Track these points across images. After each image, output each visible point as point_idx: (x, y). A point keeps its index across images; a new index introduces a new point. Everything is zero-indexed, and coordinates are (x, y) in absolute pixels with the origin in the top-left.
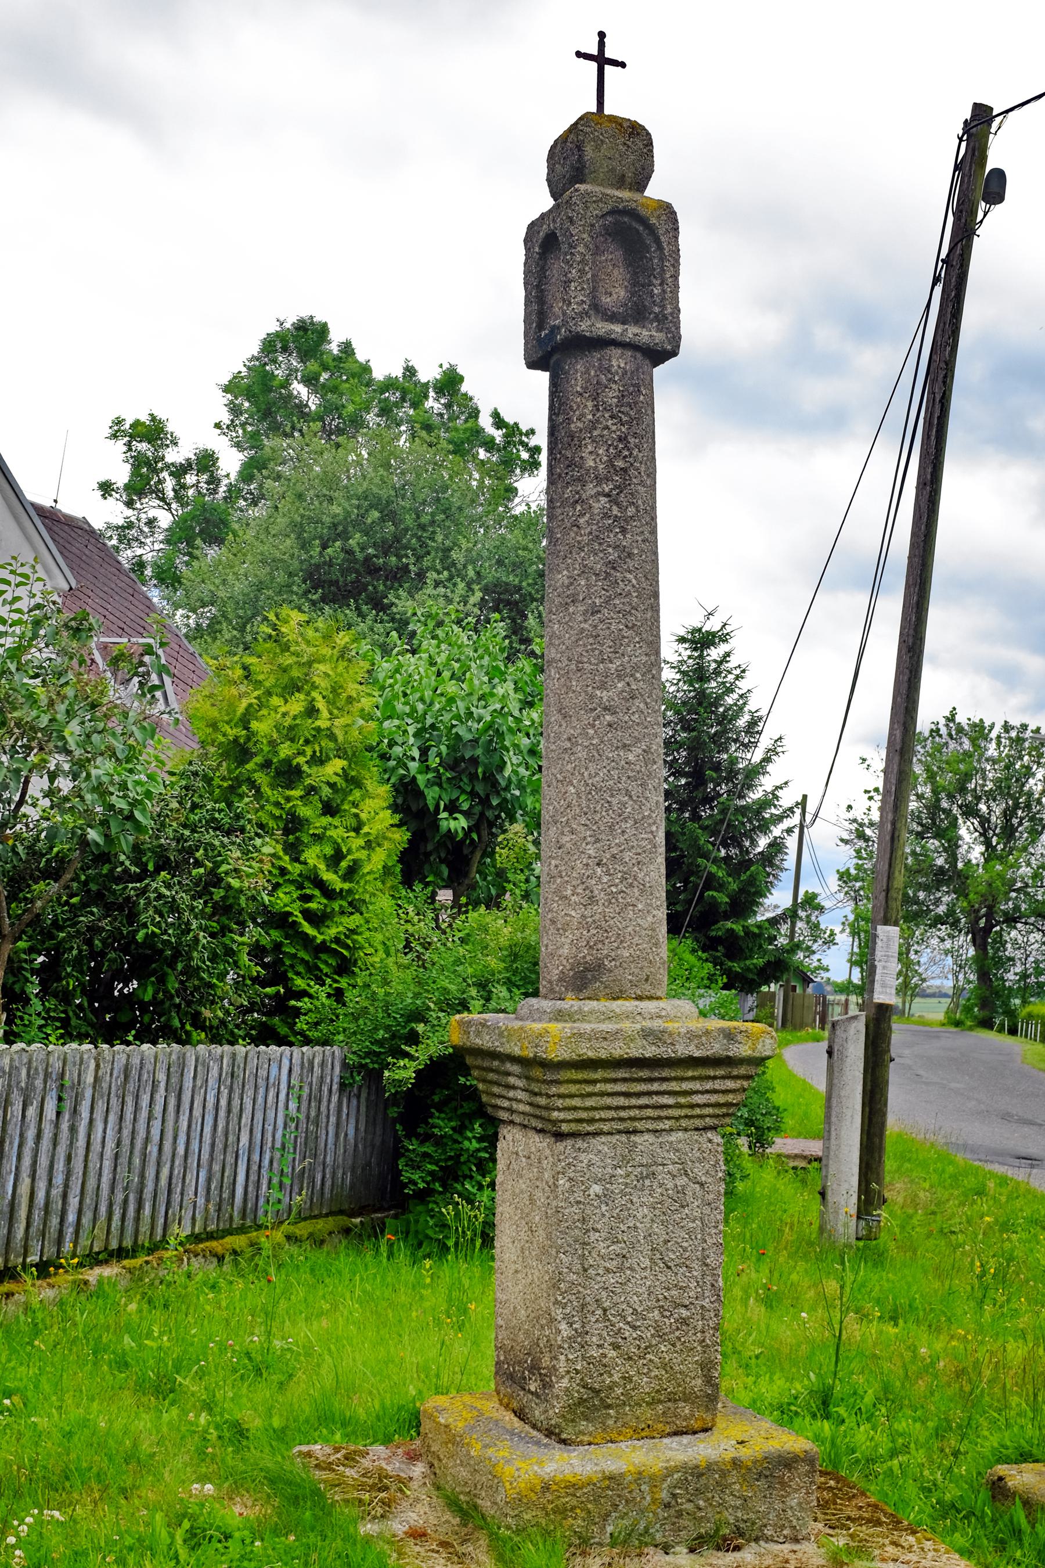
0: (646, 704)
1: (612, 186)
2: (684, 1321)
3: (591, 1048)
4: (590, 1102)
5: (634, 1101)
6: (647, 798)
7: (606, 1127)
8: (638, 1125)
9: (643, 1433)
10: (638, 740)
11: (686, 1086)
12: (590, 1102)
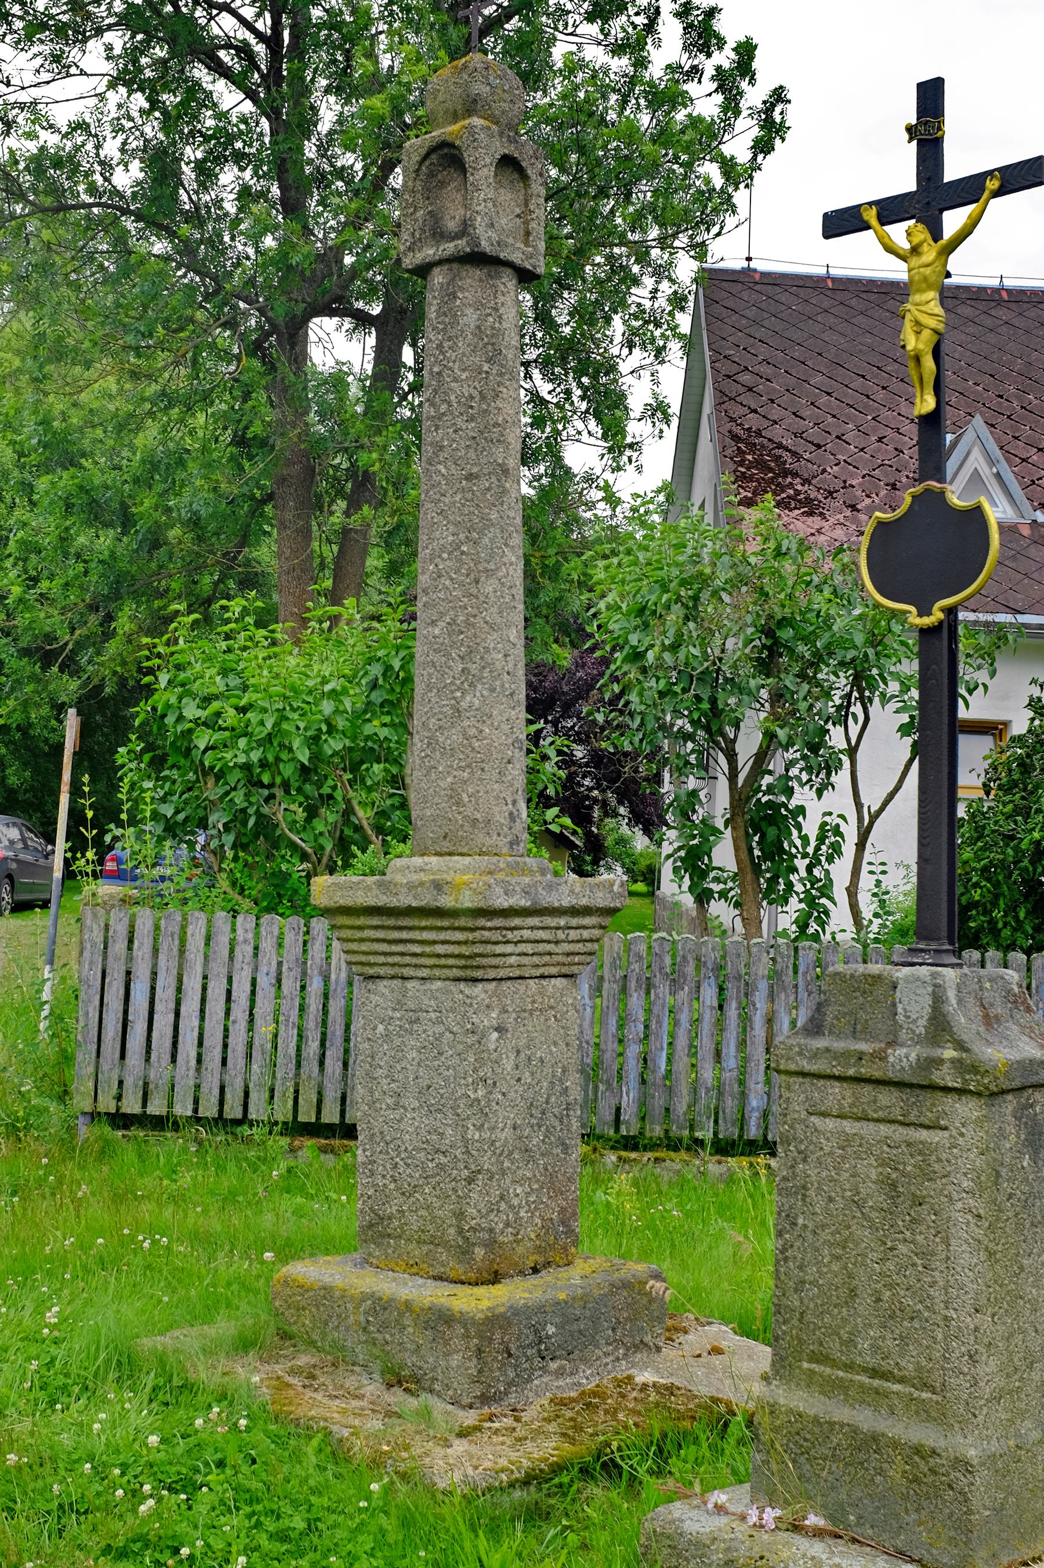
0: (452, 579)
1: (450, 124)
2: (441, 1167)
3: (342, 896)
4: (364, 947)
5: (395, 948)
6: (449, 667)
7: (382, 971)
8: (407, 972)
9: (414, 1269)
10: (442, 614)
11: (426, 935)
12: (364, 947)
